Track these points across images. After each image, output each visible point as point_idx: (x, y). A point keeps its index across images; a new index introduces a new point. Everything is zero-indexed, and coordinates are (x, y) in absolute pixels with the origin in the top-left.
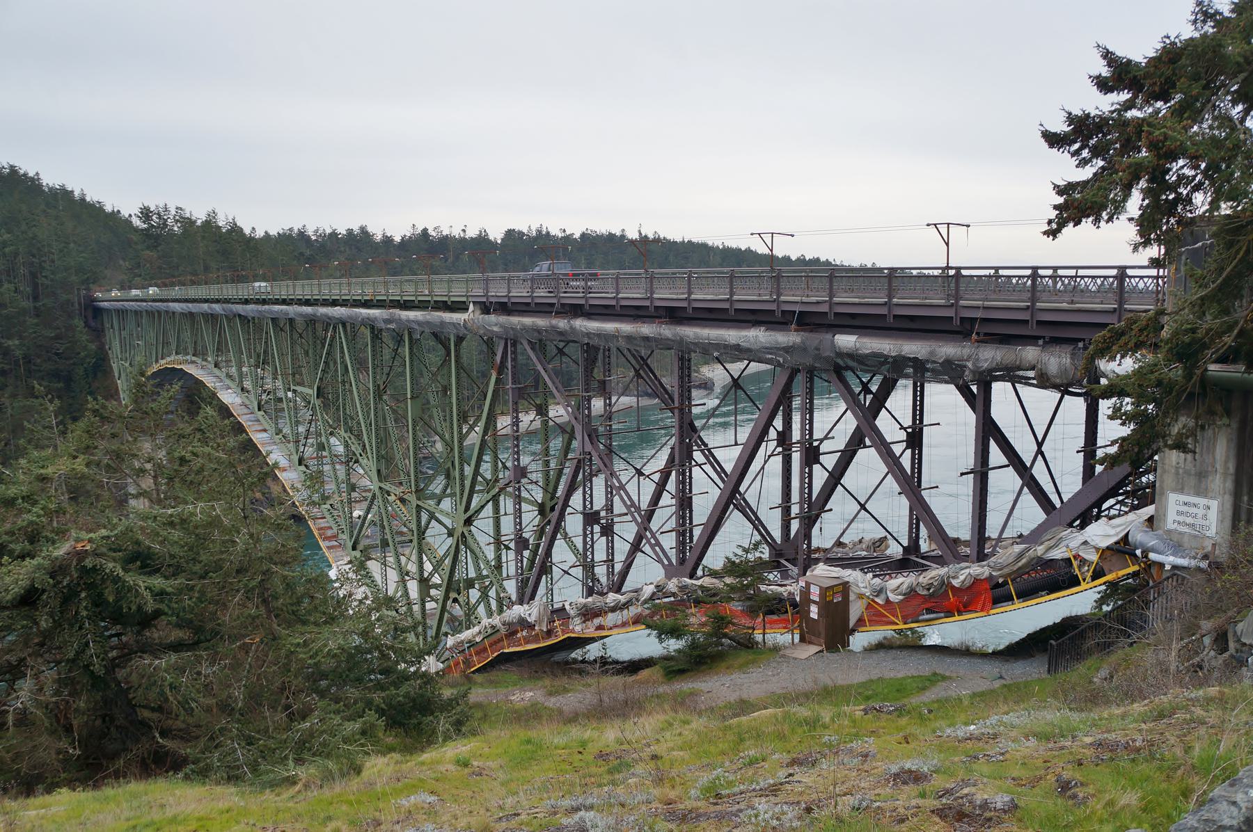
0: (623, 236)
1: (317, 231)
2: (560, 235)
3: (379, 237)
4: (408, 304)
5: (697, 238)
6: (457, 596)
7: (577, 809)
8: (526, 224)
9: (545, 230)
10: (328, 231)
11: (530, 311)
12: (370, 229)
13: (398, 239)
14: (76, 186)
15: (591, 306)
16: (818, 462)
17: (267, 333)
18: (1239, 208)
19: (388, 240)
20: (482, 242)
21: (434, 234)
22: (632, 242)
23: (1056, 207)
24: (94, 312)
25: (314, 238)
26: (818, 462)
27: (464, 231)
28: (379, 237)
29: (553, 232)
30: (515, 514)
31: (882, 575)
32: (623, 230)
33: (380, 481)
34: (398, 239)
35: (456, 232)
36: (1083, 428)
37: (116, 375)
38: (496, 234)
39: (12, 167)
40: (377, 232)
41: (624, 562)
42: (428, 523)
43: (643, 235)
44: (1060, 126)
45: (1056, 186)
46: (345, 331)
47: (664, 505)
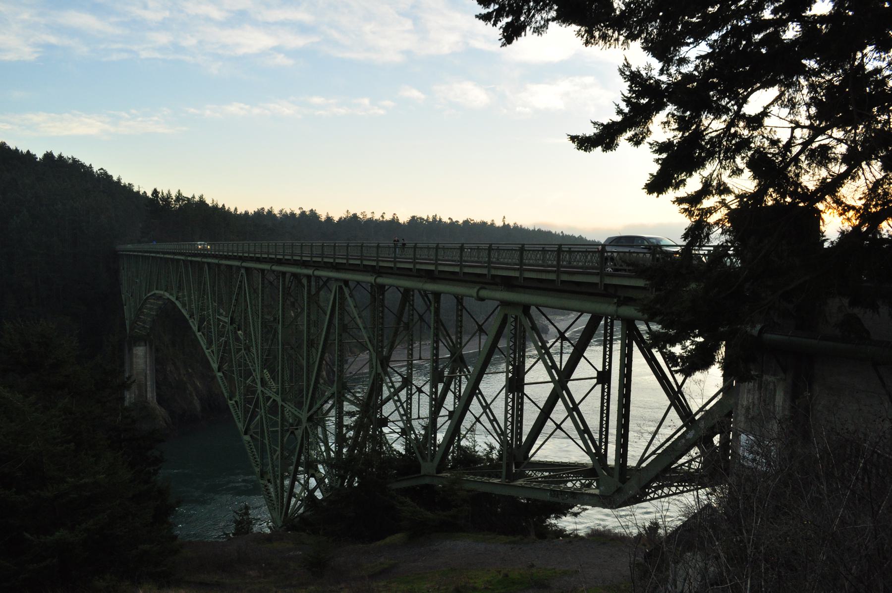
0: (492, 224)
1: (281, 211)
2: (449, 221)
3: (323, 218)
6: (314, 472)
9: (439, 217)
12: (319, 212)
13: (336, 219)
14: (425, 212)
18: (674, 181)
19: (329, 219)
21: (361, 217)
27: (382, 216)
28: (323, 218)
31: (574, 480)
32: (493, 221)
33: (262, 386)
34: (336, 219)
35: (377, 216)
37: (124, 303)
39: (74, 159)
43: (506, 223)
44: (593, 121)
46: (284, 281)
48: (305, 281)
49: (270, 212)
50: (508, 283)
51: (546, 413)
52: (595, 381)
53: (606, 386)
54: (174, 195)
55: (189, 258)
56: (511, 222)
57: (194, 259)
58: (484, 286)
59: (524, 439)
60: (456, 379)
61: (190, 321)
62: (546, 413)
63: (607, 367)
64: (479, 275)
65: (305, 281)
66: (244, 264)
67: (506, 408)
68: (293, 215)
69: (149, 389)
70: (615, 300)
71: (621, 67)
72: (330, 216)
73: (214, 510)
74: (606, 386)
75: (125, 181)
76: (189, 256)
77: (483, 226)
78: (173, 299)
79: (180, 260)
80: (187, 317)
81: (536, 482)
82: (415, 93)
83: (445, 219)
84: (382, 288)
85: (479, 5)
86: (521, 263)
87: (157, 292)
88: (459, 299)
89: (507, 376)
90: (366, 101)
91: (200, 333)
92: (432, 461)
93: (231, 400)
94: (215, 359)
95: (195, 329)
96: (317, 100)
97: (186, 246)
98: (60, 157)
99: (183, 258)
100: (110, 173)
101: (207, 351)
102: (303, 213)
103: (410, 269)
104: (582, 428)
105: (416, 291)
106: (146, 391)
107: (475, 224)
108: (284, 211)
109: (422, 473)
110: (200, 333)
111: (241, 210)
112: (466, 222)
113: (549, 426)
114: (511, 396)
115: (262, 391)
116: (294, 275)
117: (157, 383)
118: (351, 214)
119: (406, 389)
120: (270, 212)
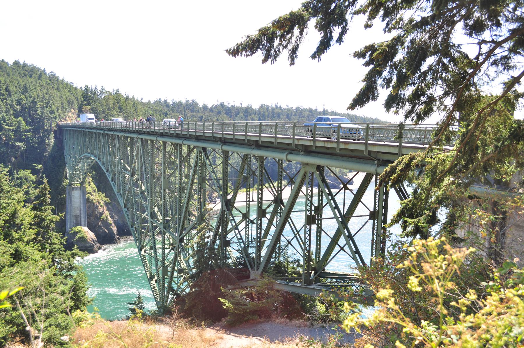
2: (286, 107)
3: (201, 105)
4: (199, 138)
11: (239, 144)
12: (198, 101)
15: (278, 143)
16: (371, 212)
19: (205, 107)
23: (81, 87)
25: (171, 103)
26: (371, 212)
27: (241, 104)
28: (201, 105)
29: (282, 107)
30: (258, 201)
34: (209, 106)
36: (357, 244)
45: (228, 52)
47: (297, 210)
48: (149, 142)
49: (165, 102)
50: (198, 138)
51: (334, 241)
52: (368, 217)
53: (376, 222)
54: (99, 89)
55: (106, 132)
57: (109, 133)
58: (291, 151)
59: (321, 257)
60: (277, 215)
61: (107, 174)
63: (377, 208)
66: (140, 136)
67: (310, 238)
68: (180, 103)
69: (82, 219)
70: (376, 162)
74: (376, 222)
75: (68, 80)
76: (106, 130)
79: (100, 133)
80: (105, 171)
81: (325, 286)
86: (196, 128)
88: (152, 141)
89: (306, 213)
91: (113, 182)
92: (257, 270)
93: (132, 227)
94: (122, 199)
95: (110, 179)
98: (24, 64)
99: (102, 132)
100: (57, 75)
101: (117, 194)
102: (187, 101)
103: (272, 143)
104: (354, 250)
106: (81, 220)
108: (175, 101)
109: (251, 278)
110: (113, 182)
111: (145, 100)
112: (298, 109)
113: (337, 248)
114: (308, 227)
115: (151, 221)
117: (88, 215)
118: (219, 103)
119: (245, 221)
120: (165, 102)
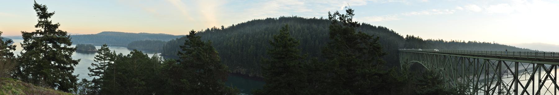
2: (479, 42)
3: (445, 42)
5: (505, 44)
7: (456, 84)
8: (472, 40)
10: (436, 40)
12: (443, 40)
17: (434, 60)
19: (446, 42)
20: (464, 43)
22: (492, 44)
24: (398, 52)
28: (445, 42)
35: (459, 41)
38: (467, 42)
40: (444, 40)
41: (529, 80)
42: (528, 85)
48: (438, 56)
51: (511, 87)
56: (495, 42)
62: (511, 87)
64: (494, 56)
65: (438, 56)
68: (437, 41)
71: (332, 14)
72: (447, 41)
73: (344, 62)
77: (392, 33)
78: (421, 63)
80: (427, 68)
82: (460, 8)
83: (478, 42)
84: (462, 57)
85: (280, 17)
87: (414, 61)
88: (478, 59)
90: (447, 10)
96: (434, 10)
97: (416, 50)
105: (502, 61)
107: (486, 43)
112: (483, 43)
116: (437, 55)
118: (452, 41)
